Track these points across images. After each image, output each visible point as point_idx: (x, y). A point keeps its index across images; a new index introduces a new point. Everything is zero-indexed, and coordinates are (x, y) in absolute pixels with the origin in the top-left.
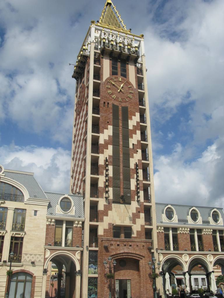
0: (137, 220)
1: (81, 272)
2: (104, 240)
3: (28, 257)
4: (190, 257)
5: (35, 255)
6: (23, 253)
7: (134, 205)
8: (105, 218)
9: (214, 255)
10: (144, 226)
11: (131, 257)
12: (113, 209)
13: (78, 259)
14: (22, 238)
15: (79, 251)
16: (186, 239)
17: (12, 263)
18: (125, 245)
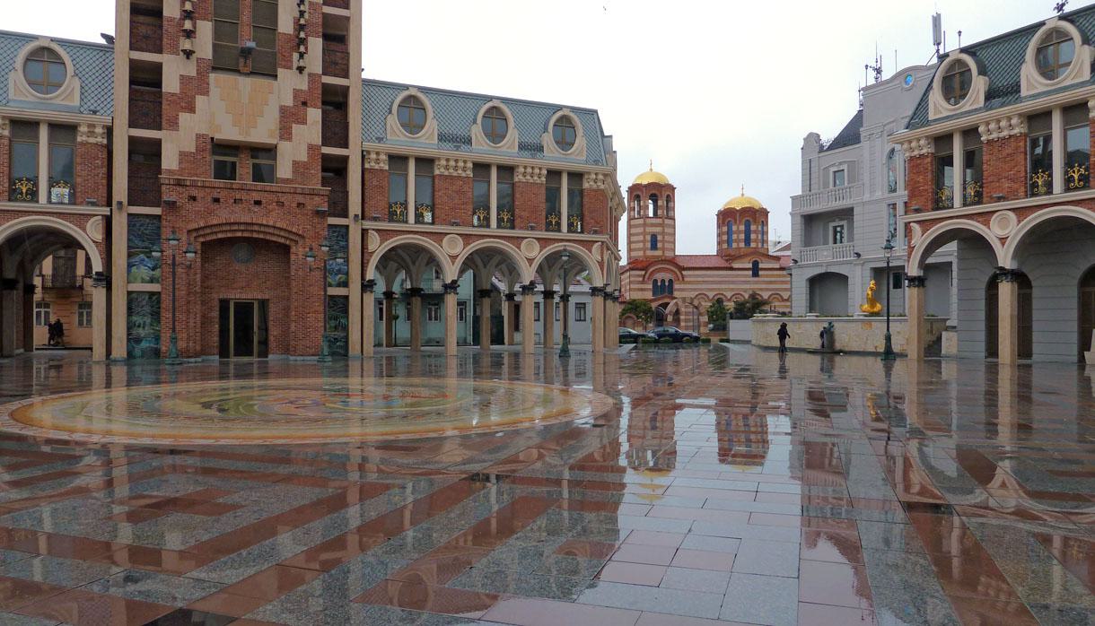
1: (106, 279)
4: (466, 245)
7: (288, 84)
8: (184, 117)
9: (544, 242)
10: (318, 148)
11: (261, 236)
12: (214, 90)
13: (94, 242)
15: (100, 217)
17: (571, 289)
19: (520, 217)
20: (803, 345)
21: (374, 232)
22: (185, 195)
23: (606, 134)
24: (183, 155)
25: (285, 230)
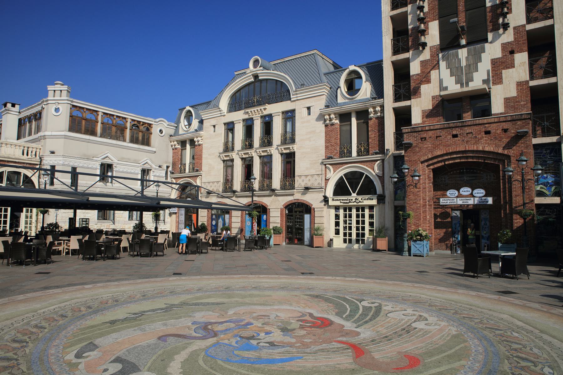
2: (406, 133)
3: (303, 181)
18: (455, 136)
20: (171, 333)
22: (419, 138)
24: (507, 101)
25: (447, 154)
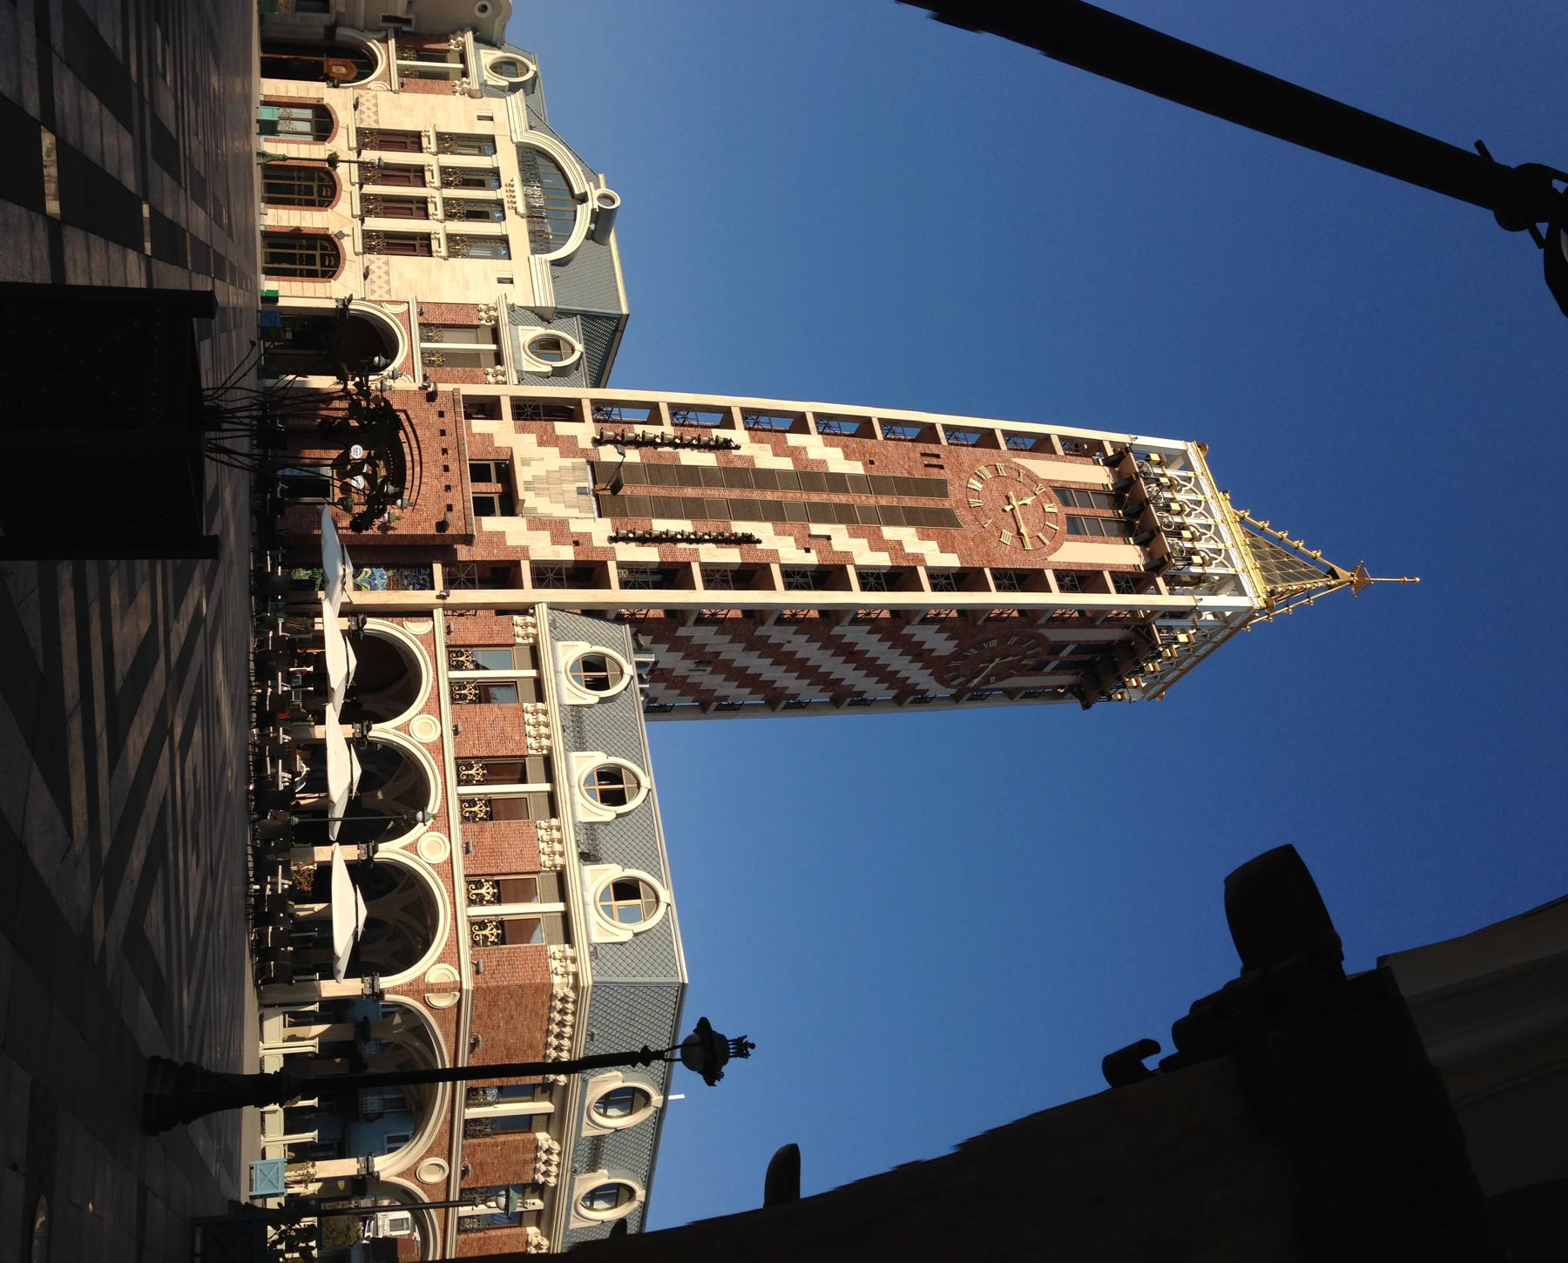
0: (545, 536)
3: (379, 268)
5: (388, 282)
6: (393, 259)
7: (600, 530)
14: (430, 253)
16: (504, 738)
19: (481, 831)
21: (432, 626)
23: (558, 469)
